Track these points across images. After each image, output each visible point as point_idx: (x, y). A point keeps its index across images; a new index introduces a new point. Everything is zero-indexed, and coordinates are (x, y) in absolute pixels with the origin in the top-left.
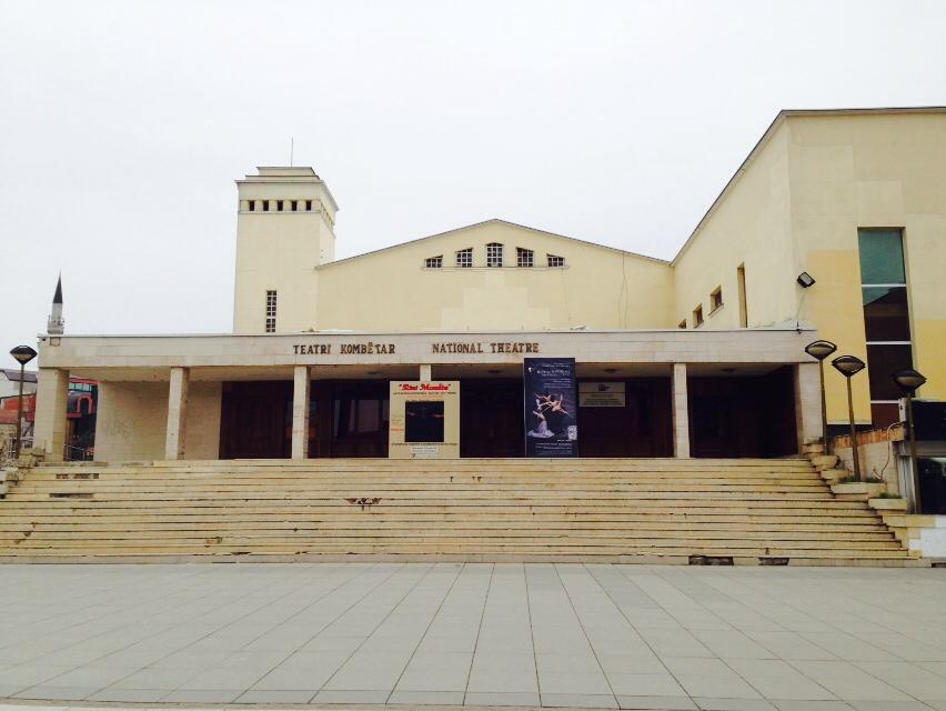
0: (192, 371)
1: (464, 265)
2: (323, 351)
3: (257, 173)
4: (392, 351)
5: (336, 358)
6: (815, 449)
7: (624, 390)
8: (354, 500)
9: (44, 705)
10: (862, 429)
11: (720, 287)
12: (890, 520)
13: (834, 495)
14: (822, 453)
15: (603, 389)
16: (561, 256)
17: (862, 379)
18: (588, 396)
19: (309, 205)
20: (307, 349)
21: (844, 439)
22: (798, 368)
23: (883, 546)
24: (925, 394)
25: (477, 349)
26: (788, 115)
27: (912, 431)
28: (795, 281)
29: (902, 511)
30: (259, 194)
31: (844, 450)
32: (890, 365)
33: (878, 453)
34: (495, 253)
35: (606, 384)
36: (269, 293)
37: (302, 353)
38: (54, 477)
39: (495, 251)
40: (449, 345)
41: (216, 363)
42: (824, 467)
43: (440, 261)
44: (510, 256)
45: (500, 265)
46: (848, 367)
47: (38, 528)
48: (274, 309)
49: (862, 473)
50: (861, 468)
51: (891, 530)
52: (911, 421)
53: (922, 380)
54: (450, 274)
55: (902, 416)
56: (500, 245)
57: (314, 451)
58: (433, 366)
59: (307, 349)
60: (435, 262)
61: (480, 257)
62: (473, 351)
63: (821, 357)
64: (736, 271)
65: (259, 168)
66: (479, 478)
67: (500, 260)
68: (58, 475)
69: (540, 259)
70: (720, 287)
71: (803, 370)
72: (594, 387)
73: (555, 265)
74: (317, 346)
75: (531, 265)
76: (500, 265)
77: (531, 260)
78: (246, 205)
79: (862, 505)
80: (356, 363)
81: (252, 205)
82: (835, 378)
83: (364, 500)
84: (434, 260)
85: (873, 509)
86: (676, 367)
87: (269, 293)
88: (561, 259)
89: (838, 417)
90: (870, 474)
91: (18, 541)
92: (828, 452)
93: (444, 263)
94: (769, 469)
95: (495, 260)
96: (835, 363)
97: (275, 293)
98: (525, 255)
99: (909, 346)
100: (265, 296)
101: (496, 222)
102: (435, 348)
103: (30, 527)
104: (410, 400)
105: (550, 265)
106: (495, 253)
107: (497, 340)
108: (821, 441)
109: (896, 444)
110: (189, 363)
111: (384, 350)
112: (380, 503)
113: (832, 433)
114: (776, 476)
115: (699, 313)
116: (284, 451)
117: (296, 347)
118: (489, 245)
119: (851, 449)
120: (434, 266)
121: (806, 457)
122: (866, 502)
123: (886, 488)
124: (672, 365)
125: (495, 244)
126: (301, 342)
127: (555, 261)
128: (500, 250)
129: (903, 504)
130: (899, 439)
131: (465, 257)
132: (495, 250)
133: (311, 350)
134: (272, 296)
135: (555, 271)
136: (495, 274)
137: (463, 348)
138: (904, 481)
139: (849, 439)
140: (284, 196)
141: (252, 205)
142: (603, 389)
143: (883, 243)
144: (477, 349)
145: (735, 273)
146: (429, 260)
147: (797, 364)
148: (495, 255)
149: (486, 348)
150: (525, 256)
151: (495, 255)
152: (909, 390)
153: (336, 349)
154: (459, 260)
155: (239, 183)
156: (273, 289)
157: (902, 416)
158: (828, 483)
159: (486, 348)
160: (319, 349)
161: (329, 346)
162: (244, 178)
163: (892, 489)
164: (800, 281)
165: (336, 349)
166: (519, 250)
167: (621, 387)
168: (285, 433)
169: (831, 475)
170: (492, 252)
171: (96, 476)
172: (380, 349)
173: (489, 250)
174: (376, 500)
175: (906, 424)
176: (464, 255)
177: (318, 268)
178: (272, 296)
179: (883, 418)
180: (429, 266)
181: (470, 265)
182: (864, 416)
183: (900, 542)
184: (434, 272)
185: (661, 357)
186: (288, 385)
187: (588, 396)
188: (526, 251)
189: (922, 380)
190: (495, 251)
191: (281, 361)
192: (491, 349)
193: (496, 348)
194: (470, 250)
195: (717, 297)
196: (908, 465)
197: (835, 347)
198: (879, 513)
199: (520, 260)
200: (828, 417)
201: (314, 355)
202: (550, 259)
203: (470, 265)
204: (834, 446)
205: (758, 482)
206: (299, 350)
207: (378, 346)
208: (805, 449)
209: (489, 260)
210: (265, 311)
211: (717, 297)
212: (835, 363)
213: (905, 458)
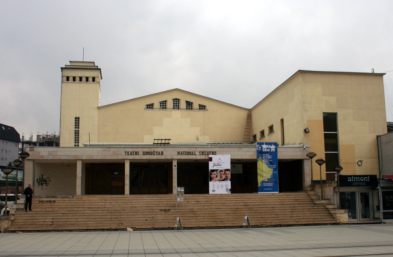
1: (163, 108)
2: (136, 154)
3: (69, 64)
4: (162, 154)
5: (141, 157)
7: (241, 167)
8: (162, 210)
10: (324, 182)
12: (332, 212)
13: (315, 204)
14: (311, 190)
16: (205, 105)
17: (324, 166)
19: (94, 79)
20: (130, 153)
21: (318, 185)
22: (304, 161)
23: (330, 219)
24: (343, 173)
25: (194, 154)
26: (301, 72)
27: (339, 184)
28: (303, 130)
29: (335, 208)
30: (72, 73)
31: (318, 190)
32: (332, 161)
33: (329, 191)
34: (176, 103)
35: (235, 165)
36: (76, 118)
37: (128, 155)
38: (38, 202)
39: (176, 102)
40: (184, 152)
42: (312, 195)
43: (152, 106)
44: (183, 105)
45: (178, 108)
46: (320, 162)
49: (324, 197)
50: (323, 195)
51: (332, 214)
52: (338, 181)
53: (342, 168)
54: (157, 113)
55: (336, 180)
56: (179, 99)
57: (324, 133)
58: (177, 159)
59: (130, 153)
60: (150, 106)
61: (170, 104)
62: (192, 154)
63: (311, 158)
64: (280, 121)
65: (70, 62)
66: (198, 201)
67: (179, 106)
68: (40, 201)
69: (196, 106)
70: (273, 124)
71: (305, 161)
73: (202, 109)
74: (133, 152)
75: (192, 109)
76: (178, 108)
77: (192, 106)
78: (65, 79)
79: (324, 207)
80: (149, 158)
81: (68, 79)
82: (316, 166)
83: (165, 210)
84: (150, 105)
85: (327, 208)
87: (76, 118)
88: (204, 106)
89: (316, 178)
90: (326, 197)
91: (51, 225)
92: (313, 190)
94: (294, 196)
95: (176, 106)
96: (316, 161)
97: (79, 118)
98: (189, 104)
99: (336, 134)
100: (74, 120)
101: (177, 90)
102: (178, 153)
104: (383, 210)
105: (200, 109)
106: (176, 103)
107: (202, 150)
108: (310, 186)
109: (334, 188)
111: (159, 154)
112: (171, 211)
113: (314, 183)
114: (297, 198)
115: (262, 133)
117: (126, 152)
118: (174, 99)
119: (321, 189)
120: (150, 108)
121: (306, 191)
122: (325, 206)
123: (331, 202)
125: (176, 99)
126: (128, 150)
127: (202, 107)
128: (179, 101)
129: (336, 207)
130: (335, 187)
131: (163, 105)
132: (176, 101)
133: (131, 154)
134: (77, 119)
135: (202, 112)
136: (176, 113)
137: (189, 153)
138: (336, 200)
139: (320, 186)
140: (80, 73)
141: (68, 79)
143: (330, 121)
144: (194, 154)
146: (147, 105)
147: (303, 160)
148: (176, 104)
149: (197, 153)
150: (189, 105)
151: (176, 104)
152: (338, 171)
154: (161, 106)
155: (62, 68)
156: (77, 116)
157: (336, 180)
158: (313, 200)
159: (197, 153)
160: (134, 154)
161: (138, 152)
162: (64, 67)
163: (332, 202)
164: (305, 130)
166: (187, 102)
167: (241, 166)
170: (175, 102)
171: (54, 201)
172: (158, 153)
173: (174, 101)
174: (169, 210)
175: (337, 182)
176: (163, 103)
177: (99, 108)
178: (77, 119)
179: (330, 177)
180: (147, 108)
181: (165, 108)
182: (324, 178)
183: (334, 218)
184: (150, 111)
188: (189, 102)
189: (342, 168)
190: (176, 102)
191: (120, 157)
192: (199, 154)
193: (201, 153)
194: (166, 101)
195: (271, 129)
196: (337, 194)
197: (316, 154)
198: (329, 210)
199: (187, 106)
200: (313, 178)
201: (133, 156)
202: (200, 106)
203: (165, 108)
204: (315, 188)
205: (292, 201)
206: (127, 153)
207: (157, 152)
209: (174, 106)
210: (74, 127)
211: (271, 129)
212: (316, 161)
213: (337, 192)
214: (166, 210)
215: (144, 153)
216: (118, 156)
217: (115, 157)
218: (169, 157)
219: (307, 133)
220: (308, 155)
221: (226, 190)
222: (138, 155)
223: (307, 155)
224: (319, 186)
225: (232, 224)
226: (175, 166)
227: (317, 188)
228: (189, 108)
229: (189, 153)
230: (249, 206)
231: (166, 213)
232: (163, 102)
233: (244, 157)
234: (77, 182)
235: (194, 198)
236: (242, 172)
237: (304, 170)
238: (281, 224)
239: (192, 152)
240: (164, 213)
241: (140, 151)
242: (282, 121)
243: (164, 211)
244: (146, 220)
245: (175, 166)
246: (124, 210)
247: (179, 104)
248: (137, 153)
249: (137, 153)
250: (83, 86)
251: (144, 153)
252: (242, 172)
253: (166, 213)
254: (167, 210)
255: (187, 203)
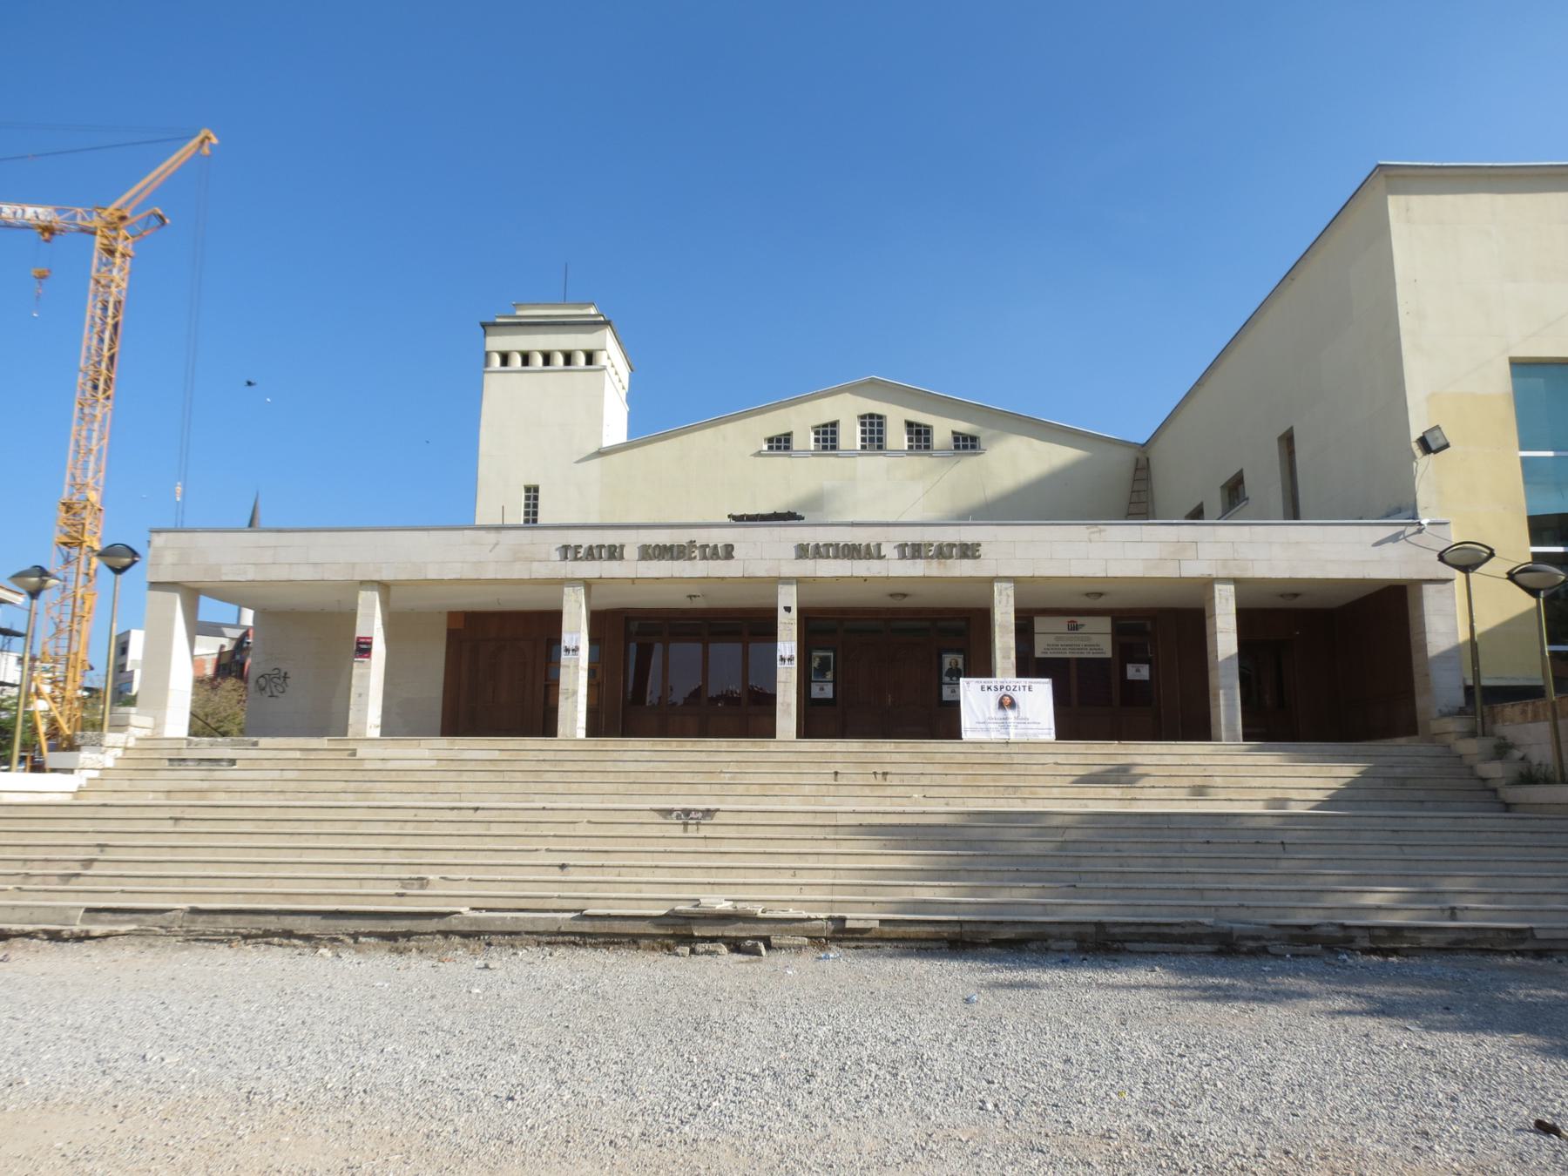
0: (394, 590)
5: (630, 567)
6: (1454, 725)
7: (1108, 629)
8: (671, 811)
9: (374, 922)
11: (1241, 471)
14: (1472, 734)
15: (1074, 627)
18: (1051, 640)
22: (1420, 590)
35: (1080, 620)
37: (576, 559)
41: (432, 574)
47: (111, 855)
48: (527, 498)
56: (880, 417)
57: (1524, 460)
66: (885, 774)
67: (880, 440)
70: (1241, 471)
72: (1061, 624)
73: (965, 447)
74: (601, 547)
76: (880, 447)
77: (927, 440)
83: (687, 812)
84: (779, 441)
86: (997, 587)
87: (528, 489)
93: (796, 444)
95: (872, 440)
97: (536, 489)
98: (918, 433)
103: (94, 854)
105: (957, 447)
108: (1461, 712)
110: (386, 575)
112: (718, 818)
116: (544, 723)
117: (880, 557)
118: (863, 417)
120: (778, 448)
121: (1432, 738)
124: (1207, 584)
125: (871, 416)
126: (574, 538)
128: (880, 424)
132: (872, 424)
136: (874, 464)
137: (852, 552)
142: (1074, 627)
145: (1274, 449)
151: (872, 432)
153: (631, 552)
156: (533, 483)
159: (889, 550)
160: (604, 553)
161: (622, 547)
165: (631, 552)
167: (1105, 624)
168: (546, 696)
169: (1494, 770)
171: (232, 762)
174: (708, 813)
178: (532, 493)
184: (780, 462)
185: (1194, 569)
186: (550, 621)
187: (1051, 640)
188: (918, 425)
191: (541, 571)
199: (910, 440)
200: (1483, 674)
201: (596, 563)
202: (956, 439)
204: (1494, 722)
207: (704, 547)
208: (1436, 726)
214: (693, 815)
215: (647, 553)
216: (535, 564)
217: (519, 572)
218: (761, 570)
219: (1436, 452)
220: (1447, 556)
221: (523, 494)
222: (622, 558)
223: (1441, 558)
224: (1524, 712)
225: (1040, 908)
226: (788, 609)
227: (1512, 721)
228: (919, 447)
229: (852, 552)
230: (1005, 845)
231: (685, 830)
232: (825, 426)
233: (1118, 570)
234: (354, 682)
235: (869, 758)
236: (1109, 654)
237: (1424, 632)
238: (1348, 922)
239: (868, 546)
240: (678, 831)
241: (632, 541)
242: (1288, 440)
243: (678, 817)
244: (563, 867)
245: (788, 609)
246: (477, 809)
247: (880, 432)
248: (614, 553)
249: (614, 553)
250: (556, 381)
251: (647, 553)
252: (1109, 654)
253: (685, 830)
254: (697, 811)
255: (830, 779)
